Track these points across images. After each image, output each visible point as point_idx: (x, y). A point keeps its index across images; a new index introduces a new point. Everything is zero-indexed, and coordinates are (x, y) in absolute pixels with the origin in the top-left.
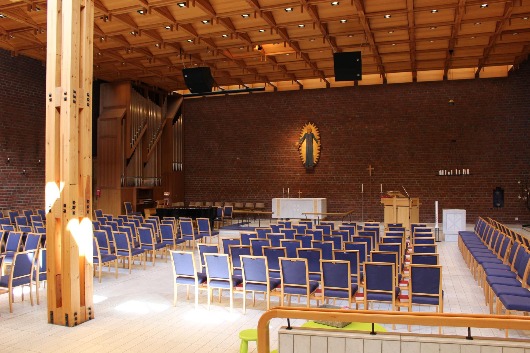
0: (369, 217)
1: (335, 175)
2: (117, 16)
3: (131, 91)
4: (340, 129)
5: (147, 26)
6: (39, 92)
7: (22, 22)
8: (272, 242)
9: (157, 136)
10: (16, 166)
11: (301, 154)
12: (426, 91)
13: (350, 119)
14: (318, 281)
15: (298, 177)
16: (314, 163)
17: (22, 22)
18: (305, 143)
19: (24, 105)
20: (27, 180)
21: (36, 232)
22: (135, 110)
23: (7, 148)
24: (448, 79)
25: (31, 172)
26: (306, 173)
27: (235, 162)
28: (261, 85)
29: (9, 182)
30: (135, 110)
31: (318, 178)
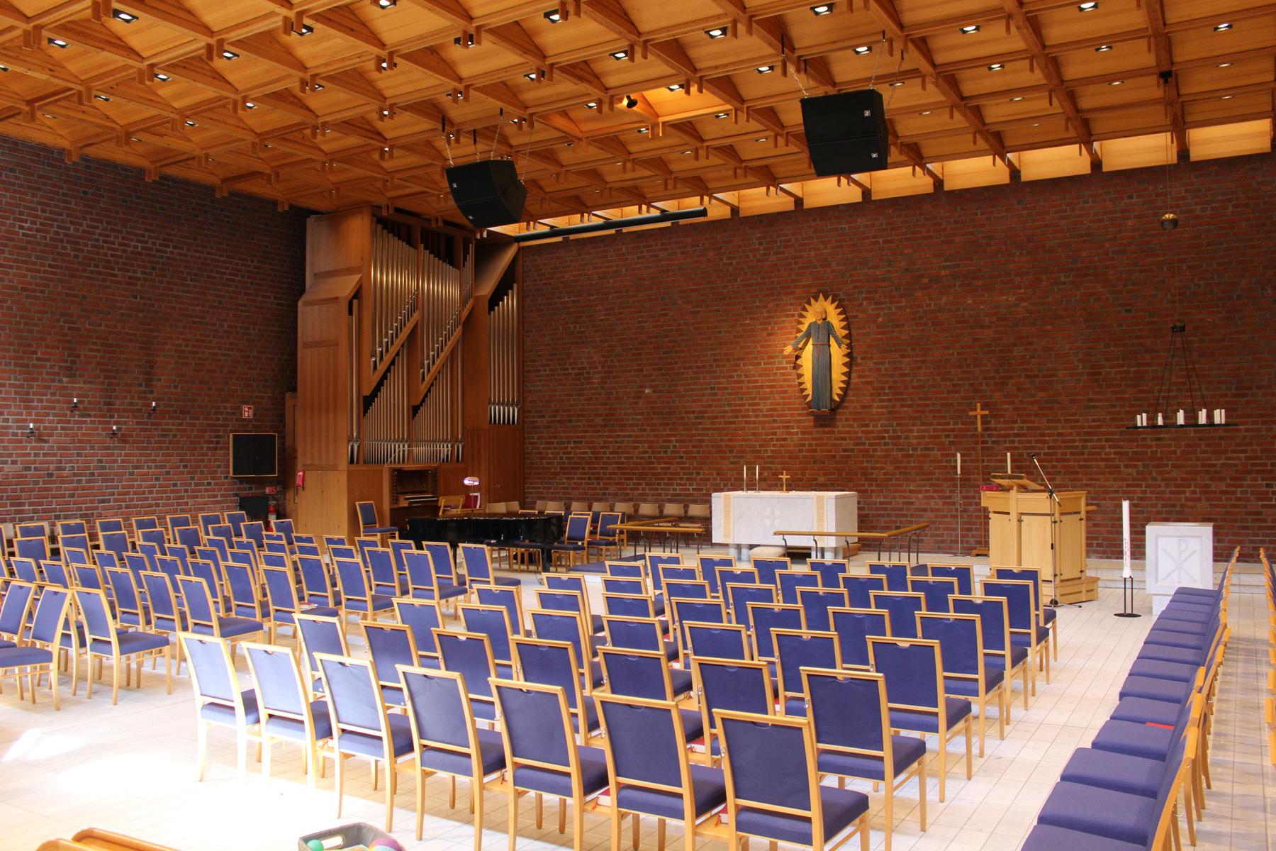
0: (977, 542)
1: (888, 432)
2: (240, 43)
3: (374, 234)
4: (899, 308)
5: (326, 65)
6: (154, 244)
7: (44, 77)
8: (850, 595)
9: (447, 338)
10: (95, 416)
11: (800, 376)
12: (1130, 197)
13: (926, 280)
14: (970, 698)
15: (796, 437)
16: (832, 400)
17: (44, 77)
18: (808, 349)
19: (116, 276)
20: (124, 448)
21: (155, 569)
22: (388, 278)
23: (72, 376)
24: (1192, 159)
25: (134, 430)
26: (815, 426)
27: (641, 401)
28: (693, 203)
29: (79, 455)
30: (388, 278)
31: (845, 439)
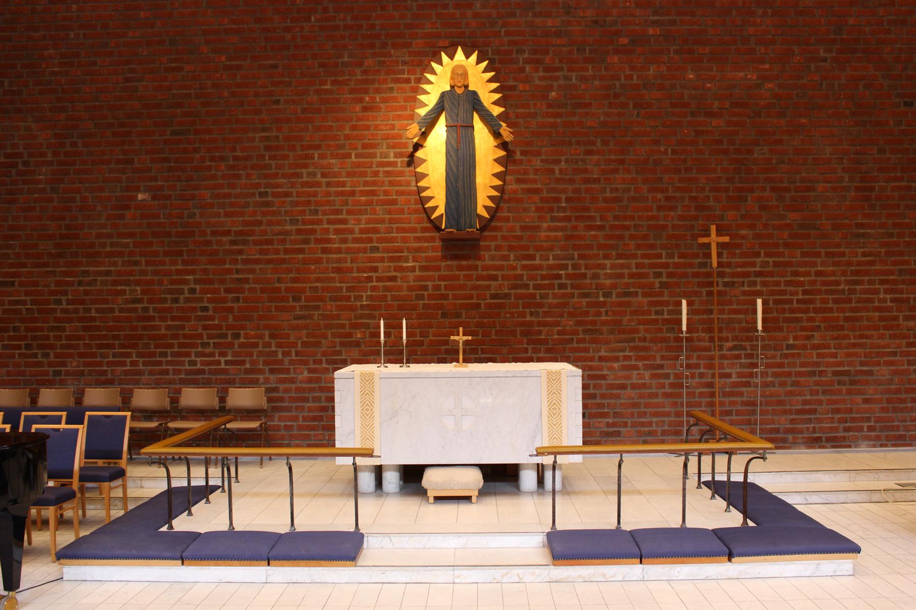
1: (565, 267)
15: (411, 275)
16: (479, 216)
26: (444, 258)
